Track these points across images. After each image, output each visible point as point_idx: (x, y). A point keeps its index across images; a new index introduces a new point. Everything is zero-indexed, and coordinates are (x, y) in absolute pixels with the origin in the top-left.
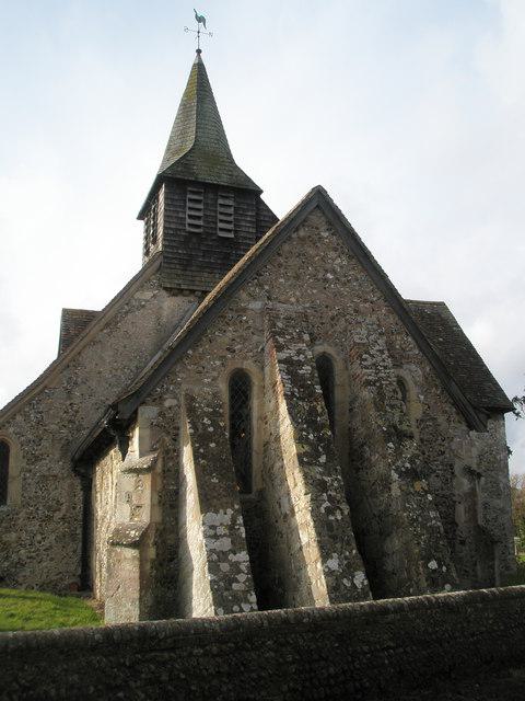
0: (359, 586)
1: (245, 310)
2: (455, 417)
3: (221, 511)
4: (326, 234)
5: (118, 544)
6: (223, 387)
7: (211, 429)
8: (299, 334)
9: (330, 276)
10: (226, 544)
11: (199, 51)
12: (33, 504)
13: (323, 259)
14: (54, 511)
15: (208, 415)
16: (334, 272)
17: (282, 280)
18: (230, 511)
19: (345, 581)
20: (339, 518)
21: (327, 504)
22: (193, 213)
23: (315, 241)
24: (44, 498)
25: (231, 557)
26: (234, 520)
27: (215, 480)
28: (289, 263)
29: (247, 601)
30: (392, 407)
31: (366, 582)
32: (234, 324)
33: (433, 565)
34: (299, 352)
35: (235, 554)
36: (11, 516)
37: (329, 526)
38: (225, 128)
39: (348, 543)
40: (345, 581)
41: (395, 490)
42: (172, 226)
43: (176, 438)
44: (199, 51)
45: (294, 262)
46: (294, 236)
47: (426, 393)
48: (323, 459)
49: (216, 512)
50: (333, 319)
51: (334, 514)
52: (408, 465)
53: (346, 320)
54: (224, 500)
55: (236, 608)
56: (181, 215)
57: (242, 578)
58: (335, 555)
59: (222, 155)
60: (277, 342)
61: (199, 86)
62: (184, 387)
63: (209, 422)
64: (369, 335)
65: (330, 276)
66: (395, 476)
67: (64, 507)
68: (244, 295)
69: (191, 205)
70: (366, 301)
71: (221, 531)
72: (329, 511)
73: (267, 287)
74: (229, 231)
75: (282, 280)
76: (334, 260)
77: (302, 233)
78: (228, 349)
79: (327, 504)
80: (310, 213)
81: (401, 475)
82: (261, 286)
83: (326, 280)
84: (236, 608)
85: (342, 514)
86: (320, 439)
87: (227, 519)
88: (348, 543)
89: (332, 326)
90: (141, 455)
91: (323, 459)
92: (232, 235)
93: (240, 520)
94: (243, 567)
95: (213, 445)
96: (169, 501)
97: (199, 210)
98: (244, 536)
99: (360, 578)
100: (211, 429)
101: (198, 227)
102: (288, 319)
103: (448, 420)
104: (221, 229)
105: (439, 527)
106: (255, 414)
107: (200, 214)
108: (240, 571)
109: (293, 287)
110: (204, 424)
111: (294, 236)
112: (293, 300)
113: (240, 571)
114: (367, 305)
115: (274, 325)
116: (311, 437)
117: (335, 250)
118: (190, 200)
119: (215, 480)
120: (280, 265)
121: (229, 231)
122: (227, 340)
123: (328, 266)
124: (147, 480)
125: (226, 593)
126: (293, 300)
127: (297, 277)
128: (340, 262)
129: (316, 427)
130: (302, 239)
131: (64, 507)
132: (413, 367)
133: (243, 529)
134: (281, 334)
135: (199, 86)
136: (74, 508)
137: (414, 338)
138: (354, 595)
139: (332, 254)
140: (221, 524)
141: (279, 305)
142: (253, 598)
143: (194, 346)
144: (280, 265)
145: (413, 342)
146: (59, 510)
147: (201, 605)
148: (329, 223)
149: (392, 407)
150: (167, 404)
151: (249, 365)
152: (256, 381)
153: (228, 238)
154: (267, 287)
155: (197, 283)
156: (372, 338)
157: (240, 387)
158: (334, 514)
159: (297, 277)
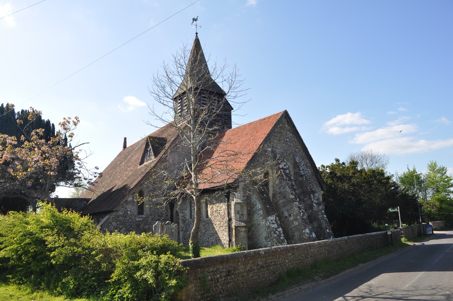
0: (314, 237)
2: (318, 186)
4: (286, 126)
8: (283, 160)
9: (288, 140)
12: (153, 214)
14: (161, 217)
16: (289, 139)
21: (302, 213)
24: (157, 212)
27: (268, 206)
28: (278, 135)
32: (264, 155)
36: (146, 219)
37: (303, 219)
40: (311, 235)
49: (271, 216)
50: (289, 154)
51: (304, 216)
52: (317, 201)
53: (293, 154)
55: (283, 244)
57: (282, 235)
58: (307, 228)
61: (197, 44)
63: (262, 188)
64: (300, 160)
65: (288, 140)
67: (164, 215)
70: (297, 148)
71: (274, 222)
82: (270, 143)
84: (283, 244)
85: (306, 216)
91: (298, 200)
94: (282, 232)
99: (314, 235)
103: (317, 187)
105: (327, 220)
108: (281, 234)
109: (279, 143)
112: (279, 148)
113: (281, 234)
114: (297, 149)
116: (294, 193)
117: (289, 131)
119: (268, 206)
120: (275, 136)
122: (262, 161)
126: (279, 148)
130: (280, 127)
131: (164, 215)
133: (279, 221)
135: (197, 44)
136: (167, 216)
137: (309, 160)
139: (288, 133)
140: (273, 220)
142: (286, 241)
145: (309, 162)
146: (162, 216)
148: (288, 122)
154: (272, 143)
156: (300, 160)
158: (304, 216)
159: (279, 140)
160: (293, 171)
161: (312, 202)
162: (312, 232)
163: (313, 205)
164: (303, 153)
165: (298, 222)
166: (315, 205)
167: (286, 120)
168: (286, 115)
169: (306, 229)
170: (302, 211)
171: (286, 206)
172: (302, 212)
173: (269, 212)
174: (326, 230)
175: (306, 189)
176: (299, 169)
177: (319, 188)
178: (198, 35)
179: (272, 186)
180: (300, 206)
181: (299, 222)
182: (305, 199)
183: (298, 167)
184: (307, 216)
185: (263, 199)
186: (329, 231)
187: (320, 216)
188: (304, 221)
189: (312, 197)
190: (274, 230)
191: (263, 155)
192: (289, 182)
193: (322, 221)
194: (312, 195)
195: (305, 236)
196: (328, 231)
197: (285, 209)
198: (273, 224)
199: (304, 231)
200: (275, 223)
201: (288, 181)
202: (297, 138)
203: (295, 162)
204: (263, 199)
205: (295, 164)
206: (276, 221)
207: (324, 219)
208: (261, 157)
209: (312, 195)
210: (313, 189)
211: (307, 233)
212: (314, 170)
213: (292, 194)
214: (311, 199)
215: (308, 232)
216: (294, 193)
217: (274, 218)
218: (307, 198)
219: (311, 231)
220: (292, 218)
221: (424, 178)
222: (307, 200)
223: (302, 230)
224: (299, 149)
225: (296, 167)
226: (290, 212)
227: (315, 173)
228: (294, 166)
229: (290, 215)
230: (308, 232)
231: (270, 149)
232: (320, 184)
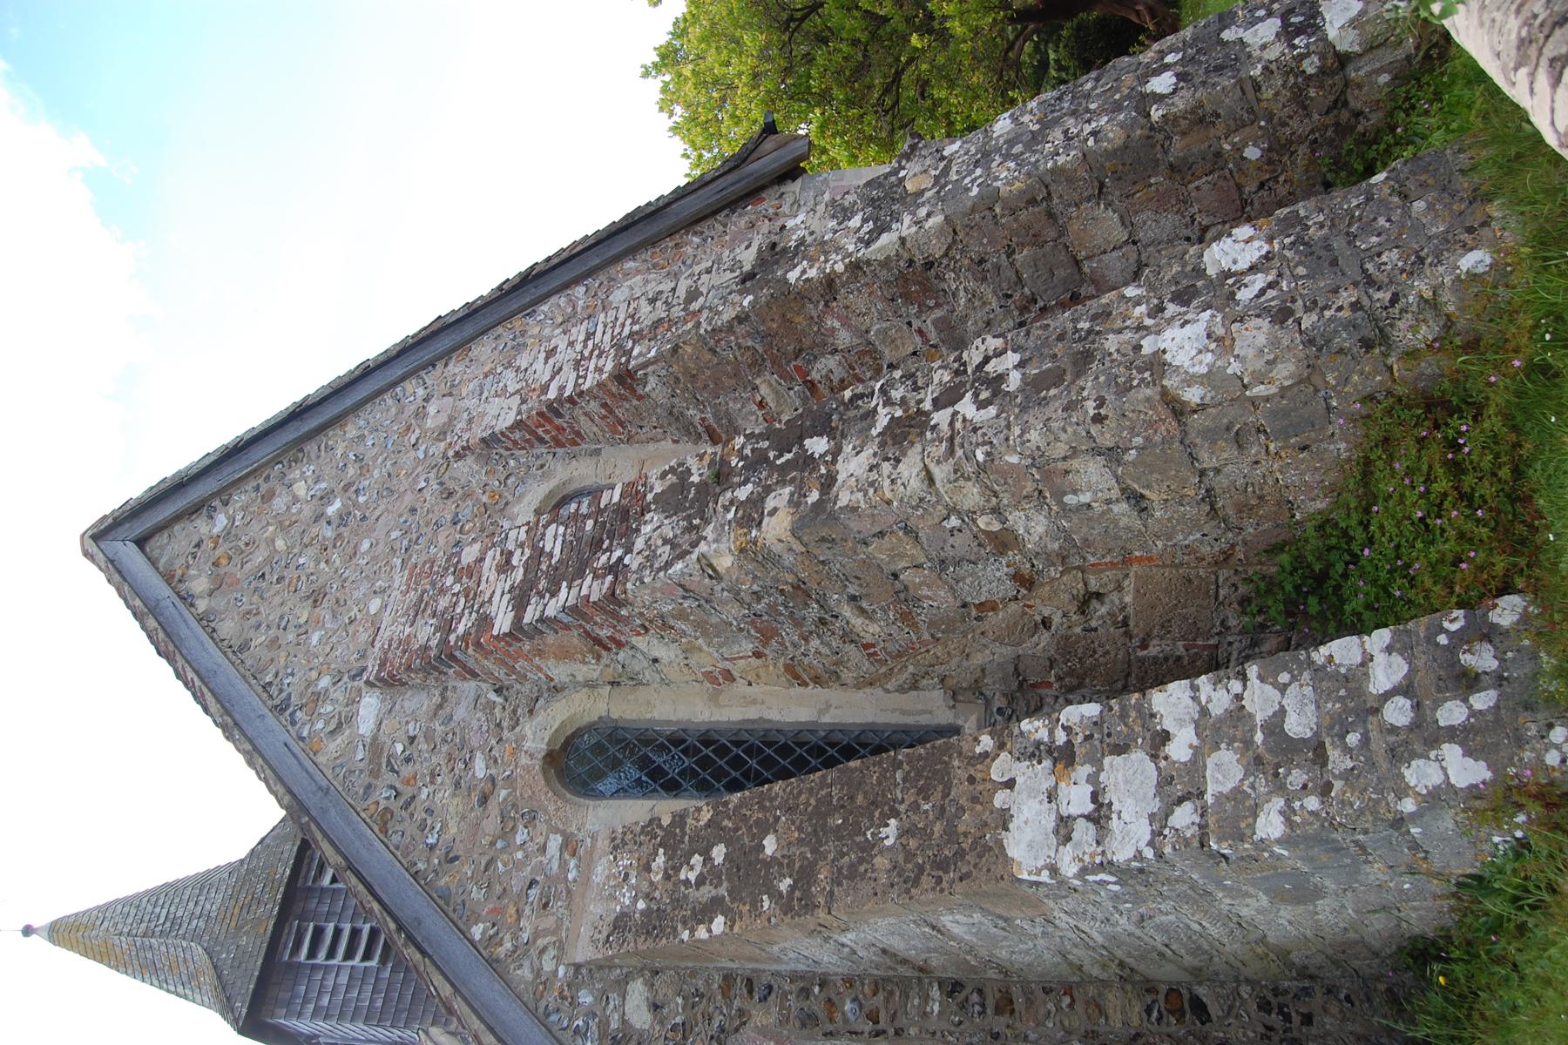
1: (375, 747)
7: (719, 853)
11: (28, 931)
15: (677, 861)
16: (326, 498)
17: (315, 638)
18: (1000, 768)
19: (1244, 295)
20: (1012, 358)
21: (966, 407)
25: (1179, 749)
26: (1035, 752)
27: (891, 831)
31: (1244, 231)
35: (1165, 737)
37: (1035, 387)
38: (181, 877)
39: (1105, 314)
44: (28, 931)
46: (202, 605)
49: (1004, 819)
51: (1001, 378)
52: (856, 222)
54: (960, 791)
56: (344, 979)
57: (1259, 697)
63: (697, 859)
69: (322, 954)
70: (421, 414)
71: (1077, 799)
73: (325, 682)
75: (315, 638)
76: (296, 500)
78: (484, 800)
80: (153, 562)
83: (343, 518)
85: (999, 353)
87: (1033, 776)
88: (1105, 314)
89: (466, 496)
91: (818, 445)
93: (1034, 728)
94: (1216, 695)
95: (770, 845)
97: (338, 932)
98: (1092, 709)
100: (719, 853)
108: (1238, 713)
110: (701, 881)
111: (202, 605)
112: (375, 605)
116: (743, 493)
117: (268, 497)
118: (312, 953)
119: (891, 831)
120: (274, 643)
123: (308, 512)
125: (1338, 761)
128: (303, 483)
139: (279, 503)
140: (1052, 796)
145: (554, 299)
148: (194, 510)
155: (157, 910)
158: (1001, 378)
159: (316, 598)
160: (607, 451)
161: (856, 267)
162: (1199, 272)
163: (886, 263)
164: (474, 353)
165: (1075, 464)
166: (885, 239)
167: (177, 528)
168: (101, 535)
169: (1158, 365)
170: (938, 404)
171: (895, 576)
172: (948, 398)
173: (951, 834)
174: (1159, 98)
175: (740, 329)
176: (570, 400)
177: (789, 199)
178: (35, 926)
179: (714, 698)
180: (882, 421)
181: (1074, 452)
182: (844, 338)
183: (559, 415)
184: (994, 343)
185: (805, 876)
186: (1167, 67)
187: (1006, 176)
188: (1055, 377)
189: (812, 273)
190: (1184, 817)
191: (408, 792)
192: (639, 543)
193: (1057, 154)
194: (792, 276)
195: (1260, 379)
196: (1162, 84)
197: (925, 591)
198: (1100, 815)
199: (1193, 395)
200: (1093, 779)
201: (629, 550)
202: (338, 420)
203: (517, 435)
204: (805, 876)
205: (542, 441)
206: (1064, 757)
207: (1036, 139)
208: (419, 815)
209: (792, 276)
210: (747, 268)
211: (1222, 343)
212: (631, 252)
213: (751, 515)
214: (830, 284)
215: (1197, 329)
216: (743, 493)
217: (1023, 772)
218: (834, 323)
219: (1183, 297)
220: (1033, 527)
221: (1302, 355)
222: (845, 322)
223: (1178, 410)
224: (426, 400)
225: (560, 429)
226: (962, 544)
227: (652, 242)
228: (559, 444)
229: (1003, 542)
230: (1197, 329)
231: (370, 707)
232: (763, 188)
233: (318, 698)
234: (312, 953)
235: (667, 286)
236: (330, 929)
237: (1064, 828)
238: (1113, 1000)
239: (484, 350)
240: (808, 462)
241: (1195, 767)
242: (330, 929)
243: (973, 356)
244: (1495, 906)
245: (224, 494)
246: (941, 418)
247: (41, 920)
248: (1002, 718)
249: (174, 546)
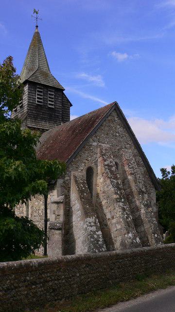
1: (91, 145)
3: (21, 201)
4: (116, 119)
5: (53, 229)
6: (84, 173)
7: (84, 188)
10: (94, 228)
13: (115, 128)
16: (118, 133)
21: (126, 215)
22: (39, 97)
23: (113, 121)
27: (88, 207)
29: (103, 248)
30: (139, 182)
33: (156, 235)
34: (111, 162)
37: (127, 222)
41: (143, 211)
42: (31, 101)
43: (69, 191)
45: (107, 128)
47: (144, 177)
48: (123, 200)
57: (101, 240)
59: (46, 75)
60: (103, 158)
62: (72, 173)
66: (143, 206)
68: (91, 140)
70: (128, 144)
71: (92, 224)
72: (127, 218)
74: (52, 105)
77: (109, 118)
79: (126, 215)
81: (144, 206)
83: (116, 136)
86: (121, 193)
87: (94, 221)
90: (58, 197)
92: (53, 107)
96: (68, 214)
100: (84, 188)
101: (41, 102)
102: (106, 150)
104: (50, 104)
106: (94, 183)
107: (42, 97)
113: (100, 238)
115: (102, 152)
116: (118, 192)
118: (38, 91)
119: (88, 207)
120: (102, 130)
121: (52, 105)
124: (62, 206)
125: (97, 245)
127: (107, 134)
129: (120, 189)
130: (109, 121)
132: (141, 168)
134: (104, 155)
138: (137, 246)
139: (118, 127)
141: (102, 144)
143: (75, 158)
144: (102, 130)
147: (81, 249)
149: (139, 182)
150: (66, 179)
151: (93, 165)
152: (95, 171)
153: (52, 108)
157: (90, 172)
159: (107, 134)
172: (127, 214)
206: (95, 223)
217: (94, 219)
229: (113, 218)
233: (97, 137)
234: (38, 91)
235: (141, 178)
236: (42, 94)
237: (90, 223)
238: (68, 226)
239: (136, 151)
240: (122, 199)
241: (95, 234)
242: (42, 94)
243: (130, 216)
244: (13, 287)
245: (120, 119)
246: (125, 213)
247: (39, 30)
248: (98, 217)
249: (114, 114)
